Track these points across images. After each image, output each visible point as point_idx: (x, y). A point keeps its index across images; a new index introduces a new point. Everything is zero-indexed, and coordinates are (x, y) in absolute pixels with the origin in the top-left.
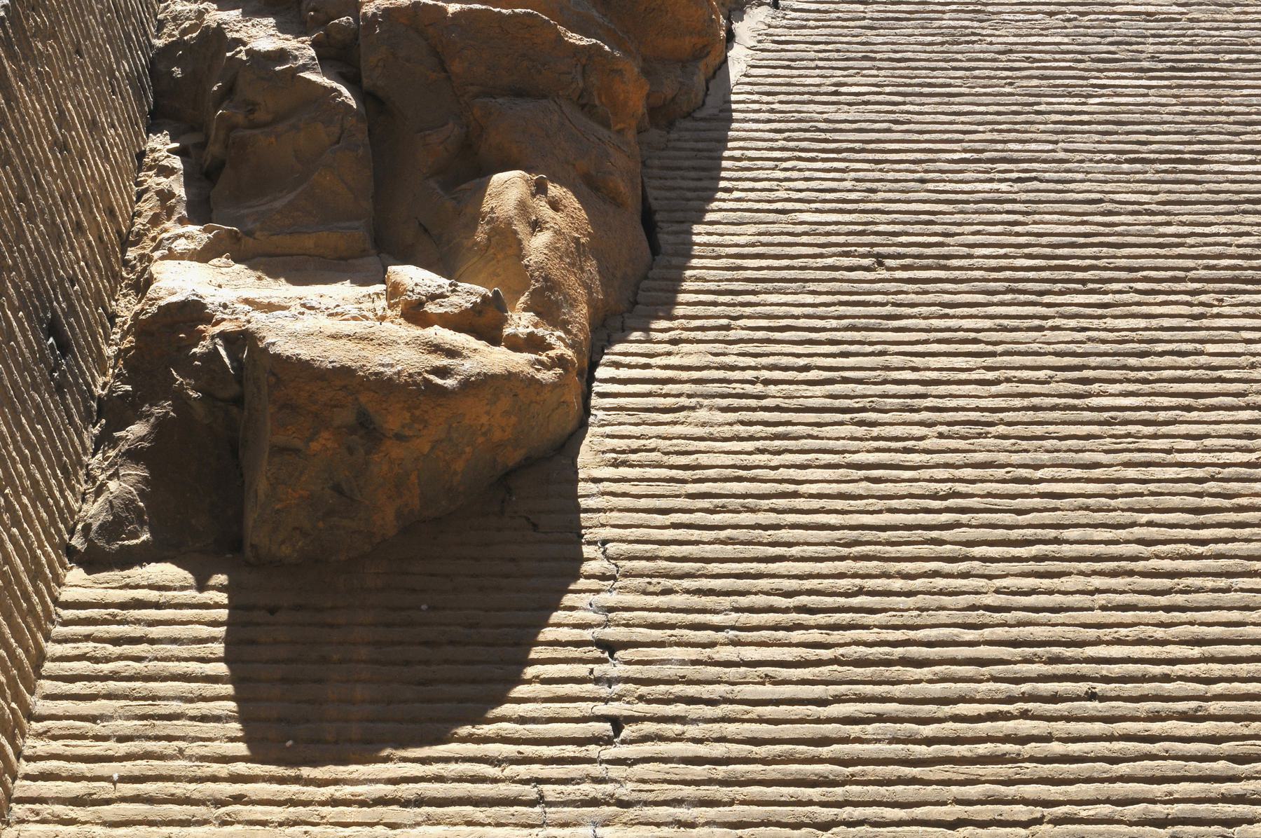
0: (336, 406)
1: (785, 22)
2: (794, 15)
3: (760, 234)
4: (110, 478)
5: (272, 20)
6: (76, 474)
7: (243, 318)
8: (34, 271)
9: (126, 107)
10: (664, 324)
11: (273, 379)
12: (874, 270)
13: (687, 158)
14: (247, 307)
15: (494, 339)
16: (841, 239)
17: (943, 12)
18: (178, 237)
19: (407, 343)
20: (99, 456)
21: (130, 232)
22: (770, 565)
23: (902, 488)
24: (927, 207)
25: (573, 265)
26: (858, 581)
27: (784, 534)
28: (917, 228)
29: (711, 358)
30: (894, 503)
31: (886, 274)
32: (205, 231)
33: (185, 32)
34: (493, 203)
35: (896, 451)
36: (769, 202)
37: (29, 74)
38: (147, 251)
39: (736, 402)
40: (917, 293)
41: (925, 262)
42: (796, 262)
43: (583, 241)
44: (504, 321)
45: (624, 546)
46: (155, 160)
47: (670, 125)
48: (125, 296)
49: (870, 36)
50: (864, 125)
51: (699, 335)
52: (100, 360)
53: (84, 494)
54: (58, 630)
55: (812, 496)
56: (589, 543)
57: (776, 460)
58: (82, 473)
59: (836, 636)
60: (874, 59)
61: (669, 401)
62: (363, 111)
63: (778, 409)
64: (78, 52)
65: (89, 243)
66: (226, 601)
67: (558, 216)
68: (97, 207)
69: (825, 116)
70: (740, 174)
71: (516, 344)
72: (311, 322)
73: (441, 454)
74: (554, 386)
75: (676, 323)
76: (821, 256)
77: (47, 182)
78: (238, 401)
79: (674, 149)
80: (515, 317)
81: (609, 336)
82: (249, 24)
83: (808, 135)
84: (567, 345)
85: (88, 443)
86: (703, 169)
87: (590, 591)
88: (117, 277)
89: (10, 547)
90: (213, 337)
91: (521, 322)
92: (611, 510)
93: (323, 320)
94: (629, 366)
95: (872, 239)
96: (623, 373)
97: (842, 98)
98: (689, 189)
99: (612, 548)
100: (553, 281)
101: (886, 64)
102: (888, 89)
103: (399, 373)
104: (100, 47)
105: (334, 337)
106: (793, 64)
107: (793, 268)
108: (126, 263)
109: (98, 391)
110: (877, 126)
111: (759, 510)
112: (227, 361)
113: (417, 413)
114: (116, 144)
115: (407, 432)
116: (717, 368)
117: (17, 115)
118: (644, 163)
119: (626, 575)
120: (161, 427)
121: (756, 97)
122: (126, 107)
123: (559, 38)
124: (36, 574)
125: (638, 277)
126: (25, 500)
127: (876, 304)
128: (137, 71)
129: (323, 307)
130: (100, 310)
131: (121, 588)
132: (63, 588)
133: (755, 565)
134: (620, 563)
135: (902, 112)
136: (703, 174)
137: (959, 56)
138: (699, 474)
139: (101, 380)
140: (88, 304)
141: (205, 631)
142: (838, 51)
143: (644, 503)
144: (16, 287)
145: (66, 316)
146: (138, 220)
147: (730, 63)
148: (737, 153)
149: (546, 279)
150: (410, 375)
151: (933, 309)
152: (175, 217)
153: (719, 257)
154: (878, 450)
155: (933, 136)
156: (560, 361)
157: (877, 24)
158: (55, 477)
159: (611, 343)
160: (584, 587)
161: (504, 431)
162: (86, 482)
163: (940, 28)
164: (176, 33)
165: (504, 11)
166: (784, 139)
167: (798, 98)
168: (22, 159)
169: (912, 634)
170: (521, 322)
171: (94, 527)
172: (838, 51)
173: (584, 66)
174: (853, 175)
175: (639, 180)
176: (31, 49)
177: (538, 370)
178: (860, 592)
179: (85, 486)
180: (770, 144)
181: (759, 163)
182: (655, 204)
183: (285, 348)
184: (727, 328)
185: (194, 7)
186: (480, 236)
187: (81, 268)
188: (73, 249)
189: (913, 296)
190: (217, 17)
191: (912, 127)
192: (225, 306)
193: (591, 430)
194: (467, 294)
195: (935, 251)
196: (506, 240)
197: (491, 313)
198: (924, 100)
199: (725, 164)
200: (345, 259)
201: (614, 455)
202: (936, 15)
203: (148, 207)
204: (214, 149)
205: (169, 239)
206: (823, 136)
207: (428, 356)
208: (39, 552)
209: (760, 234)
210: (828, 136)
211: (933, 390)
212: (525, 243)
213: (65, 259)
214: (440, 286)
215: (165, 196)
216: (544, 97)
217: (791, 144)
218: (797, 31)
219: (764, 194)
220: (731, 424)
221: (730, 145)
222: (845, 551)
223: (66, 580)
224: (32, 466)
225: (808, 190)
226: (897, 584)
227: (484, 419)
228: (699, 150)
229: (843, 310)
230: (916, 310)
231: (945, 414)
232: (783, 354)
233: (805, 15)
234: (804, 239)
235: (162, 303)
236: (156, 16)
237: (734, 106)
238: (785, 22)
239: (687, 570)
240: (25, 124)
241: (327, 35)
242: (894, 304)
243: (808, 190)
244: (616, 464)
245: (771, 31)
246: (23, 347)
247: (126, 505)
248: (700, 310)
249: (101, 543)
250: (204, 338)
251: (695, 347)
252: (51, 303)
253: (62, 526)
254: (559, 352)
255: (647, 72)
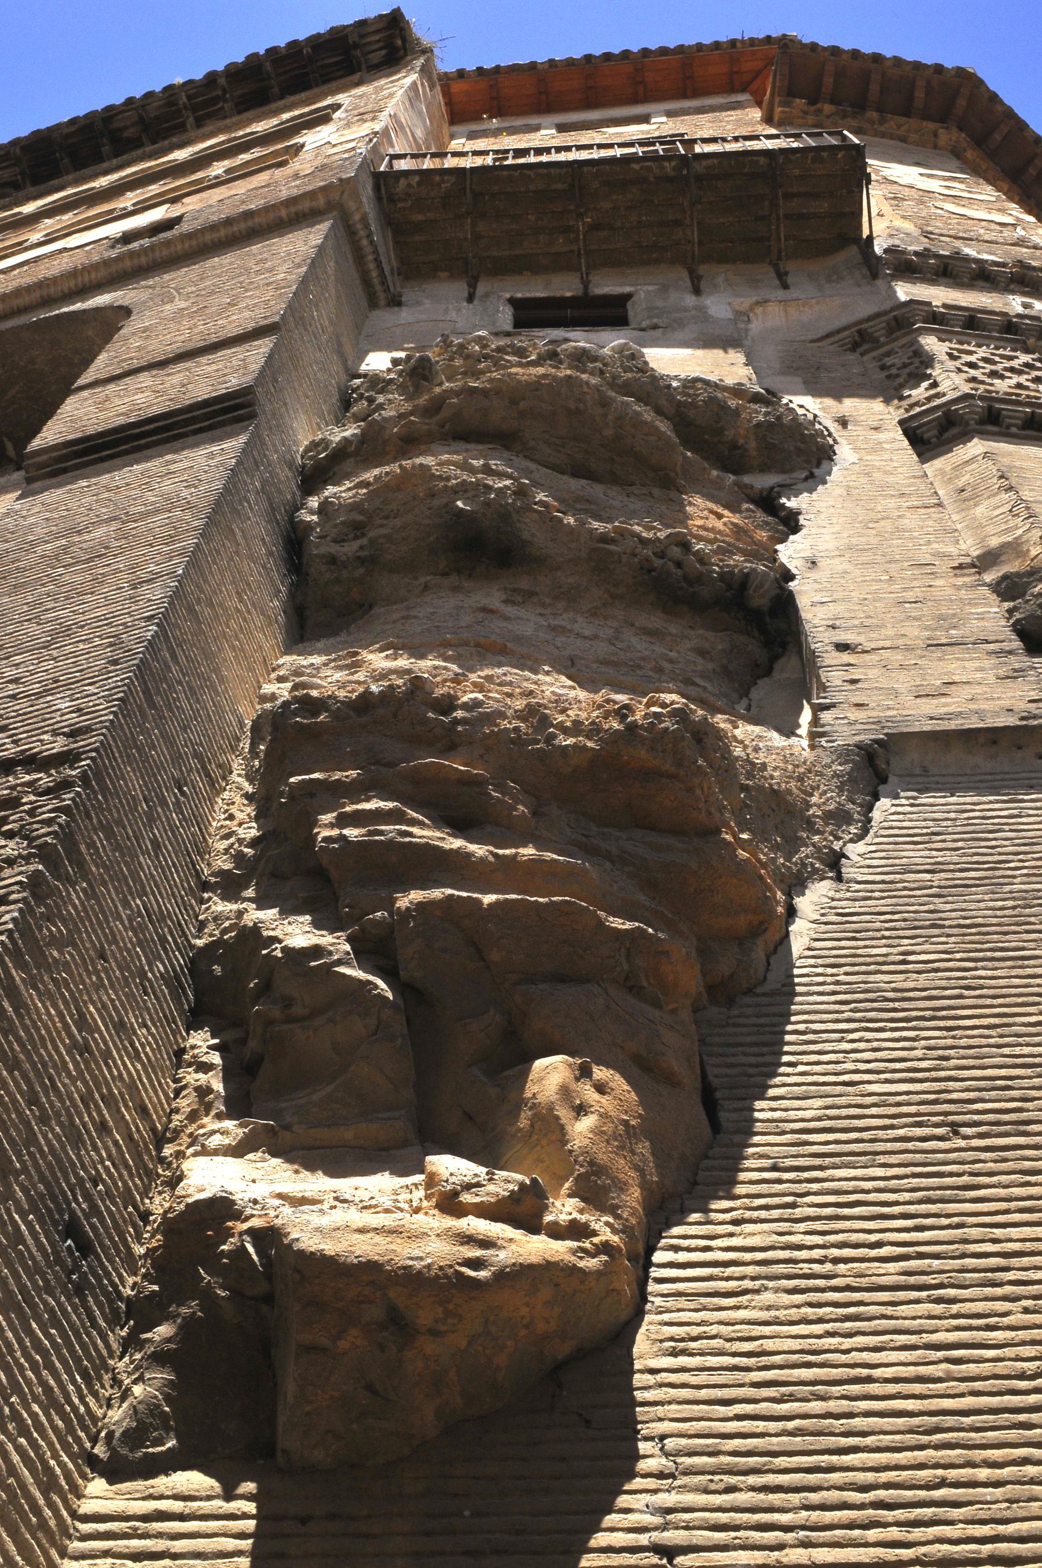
0: (362, 1302)
1: (849, 894)
2: (858, 887)
3: (827, 1108)
4: (135, 1382)
5: (308, 917)
6: (100, 1379)
7: (272, 1213)
8: (47, 1173)
9: (161, 1007)
10: (725, 1204)
11: (297, 1277)
12: (949, 1139)
13: (749, 1034)
14: (277, 1202)
15: (531, 1224)
16: (913, 1109)
17: (1014, 877)
18: (213, 1132)
19: (438, 1235)
20: (126, 1359)
21: (166, 1129)
22: (843, 1457)
23: (986, 1368)
24: (1003, 1072)
25: (622, 1147)
26: (940, 1472)
27: (857, 1423)
28: (993, 1094)
29: (775, 1237)
30: (978, 1385)
31: (962, 1143)
32: (241, 1126)
33: (225, 931)
34: (535, 1089)
35: (978, 1328)
36: (836, 1074)
37: (43, 982)
38: (183, 1148)
39: (803, 1283)
40: (995, 1161)
41: (1003, 1128)
42: (865, 1135)
43: (633, 1123)
44: (544, 1208)
45: (684, 1441)
46: (194, 1057)
47: (731, 1002)
48: (160, 1193)
49: (938, 903)
50: (934, 993)
51: (763, 1214)
52: (131, 1262)
53: (110, 1399)
54: (76, 1546)
55: (887, 1381)
56: (646, 1439)
57: (847, 1343)
58: (107, 1377)
59: (917, 1533)
60: (943, 927)
61: (732, 1285)
62: (401, 1002)
63: (849, 1288)
64: (103, 956)
65: (116, 1143)
66: (254, 1512)
67: (604, 1100)
68: (126, 1106)
69: (893, 985)
70: (804, 1048)
71: (556, 1232)
72: (340, 1216)
73: (480, 1349)
74: (599, 1274)
75: (738, 1203)
76: (892, 1127)
77: (64, 1085)
78: (269, 1299)
79: (735, 1025)
80: (558, 1203)
81: (667, 1219)
82: (286, 922)
83: (875, 1005)
84: (614, 1231)
85: (115, 1346)
86: (765, 1044)
87: (647, 1491)
88: (151, 1175)
89: (16, 1458)
90: (241, 1234)
91: (564, 1208)
92: (670, 1403)
93: (357, 1214)
94: (689, 1249)
95: (945, 1107)
96: (682, 1257)
97: (910, 967)
98: (751, 1065)
99: (670, 1443)
100: (599, 1166)
101: (955, 931)
102: (958, 956)
103: (429, 1266)
104: (128, 951)
105: (361, 1231)
106: (858, 935)
107: (862, 1141)
108: (162, 1160)
109: (128, 1292)
110: (948, 992)
111: (830, 1398)
112: (255, 1257)
113: (451, 1307)
114: (149, 1044)
115: (443, 1328)
116: (783, 1248)
117: (28, 1022)
118: (702, 1042)
119: (688, 1472)
120: (187, 1329)
121: (820, 970)
122: (161, 1007)
123: (600, 923)
124: (49, 1485)
125: (695, 1155)
126: (36, 1408)
127: (951, 1175)
128: (174, 970)
129: (357, 1199)
130: (130, 1209)
131: (144, 1499)
132: (83, 1500)
133: (826, 1457)
134: (680, 1460)
135: (974, 978)
136: (765, 1049)
137: (1032, 919)
138: (765, 1360)
139: (130, 1280)
140: (115, 1204)
141: (231, 1544)
142: (905, 920)
143: (704, 1394)
144: (25, 1190)
145: (87, 1217)
146: (175, 1117)
147: (792, 937)
148: (801, 1027)
149: (592, 1163)
150: (441, 1268)
151: (1013, 1177)
152: (213, 1113)
153: (783, 1133)
154: (958, 1328)
155: (1008, 1000)
156: (606, 1248)
157: (945, 891)
158: (74, 1382)
159: (669, 1226)
160: (641, 1487)
161: (548, 1322)
162: (112, 1387)
163: (1011, 892)
164: (217, 932)
165: (541, 900)
166: (851, 1011)
167: (864, 968)
168: (34, 1064)
169: (1001, 1529)
170: (564, 1208)
171: (117, 1435)
172: (905, 920)
173: (628, 949)
174: (923, 1042)
175: (697, 1059)
176: (45, 958)
177: (581, 1258)
178: (943, 1483)
179: (110, 1391)
180: (835, 1016)
181: (825, 1036)
182: (715, 1082)
183: (309, 1243)
184: (793, 1206)
185: (235, 907)
186: (523, 1123)
187: (107, 1169)
188: (96, 1148)
189: (992, 1165)
190: (254, 917)
191: (985, 991)
192: (255, 1202)
193: (648, 1318)
194: (505, 1182)
195: (1013, 1117)
196: (549, 1126)
197: (529, 1201)
198: (997, 964)
199: (788, 1038)
200: (386, 1149)
201: (673, 1344)
202: (1006, 880)
203: (186, 1103)
204: (253, 1044)
205: (204, 1135)
206: (891, 1005)
207: (461, 1248)
208: (52, 1462)
209: (827, 1108)
210: (897, 1005)
211: (1015, 1262)
212: (568, 1128)
213: (86, 1160)
214: (476, 1175)
215: (203, 1091)
216: (588, 981)
217: (858, 1015)
218: (862, 903)
219: (829, 1066)
220: (798, 1307)
221: (793, 1019)
222: (925, 1439)
223: (87, 1492)
224: (45, 1373)
225: (876, 1060)
226: (983, 1474)
227: (524, 1311)
228: (762, 1026)
229: (915, 1182)
230: (995, 1179)
231: (1030, 1288)
232: (855, 1231)
233: (869, 887)
234: (874, 1111)
235: (190, 1200)
236: (197, 917)
237: (797, 980)
238: (849, 894)
239: (752, 1465)
240: (37, 1030)
241: (363, 930)
242: (971, 1174)
243: (876, 1060)
244: (674, 1353)
245: (835, 904)
246: (34, 1250)
247: (151, 1410)
248: (764, 1188)
249: (124, 1451)
250: (232, 1235)
251: (759, 1227)
252: (69, 1204)
253: (82, 1434)
254: (604, 1238)
255: (703, 952)
